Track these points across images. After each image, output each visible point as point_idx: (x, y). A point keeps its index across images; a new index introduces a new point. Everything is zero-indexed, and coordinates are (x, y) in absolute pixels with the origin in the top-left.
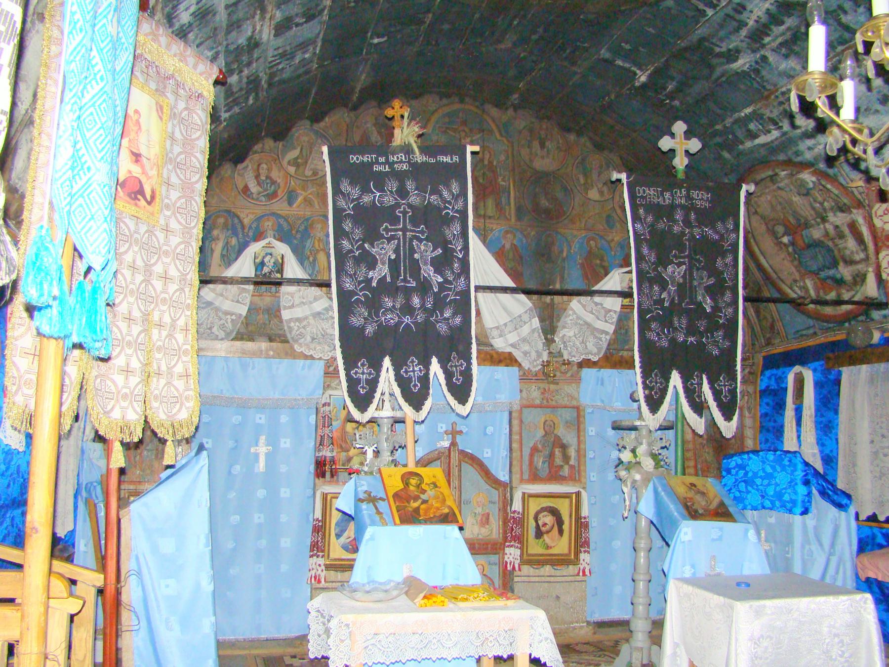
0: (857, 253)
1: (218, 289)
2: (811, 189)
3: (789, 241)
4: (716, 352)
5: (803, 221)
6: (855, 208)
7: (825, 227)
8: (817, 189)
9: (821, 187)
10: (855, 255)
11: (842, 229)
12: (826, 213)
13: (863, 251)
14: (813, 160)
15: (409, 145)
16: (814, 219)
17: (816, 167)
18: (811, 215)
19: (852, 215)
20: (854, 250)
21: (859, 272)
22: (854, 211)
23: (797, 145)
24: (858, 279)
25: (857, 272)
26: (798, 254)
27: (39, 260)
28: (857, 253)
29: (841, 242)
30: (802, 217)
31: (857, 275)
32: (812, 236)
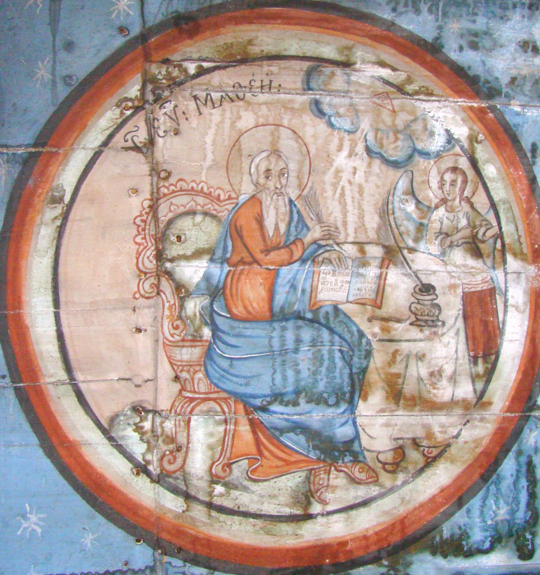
0: (453, 379)
1: (452, 298)
2: (425, 154)
3: (207, 278)
4: (527, 552)
5: (316, 233)
6: (518, 255)
7: (381, 278)
8: (448, 163)
9: (464, 163)
10: (444, 382)
11: (440, 301)
12: (417, 240)
13: (474, 378)
14: (505, 80)
15: (532, 51)
16: (360, 245)
17: (498, 103)
18: (361, 226)
19: (499, 275)
20: (448, 370)
21: (430, 435)
22: (512, 263)
23: (504, 18)
24: (414, 455)
25: (420, 433)
26: (215, 329)
27: (356, 204)
28: (453, 379)
29: (415, 333)
30: (320, 220)
31: (415, 443)
32: (314, 290)
